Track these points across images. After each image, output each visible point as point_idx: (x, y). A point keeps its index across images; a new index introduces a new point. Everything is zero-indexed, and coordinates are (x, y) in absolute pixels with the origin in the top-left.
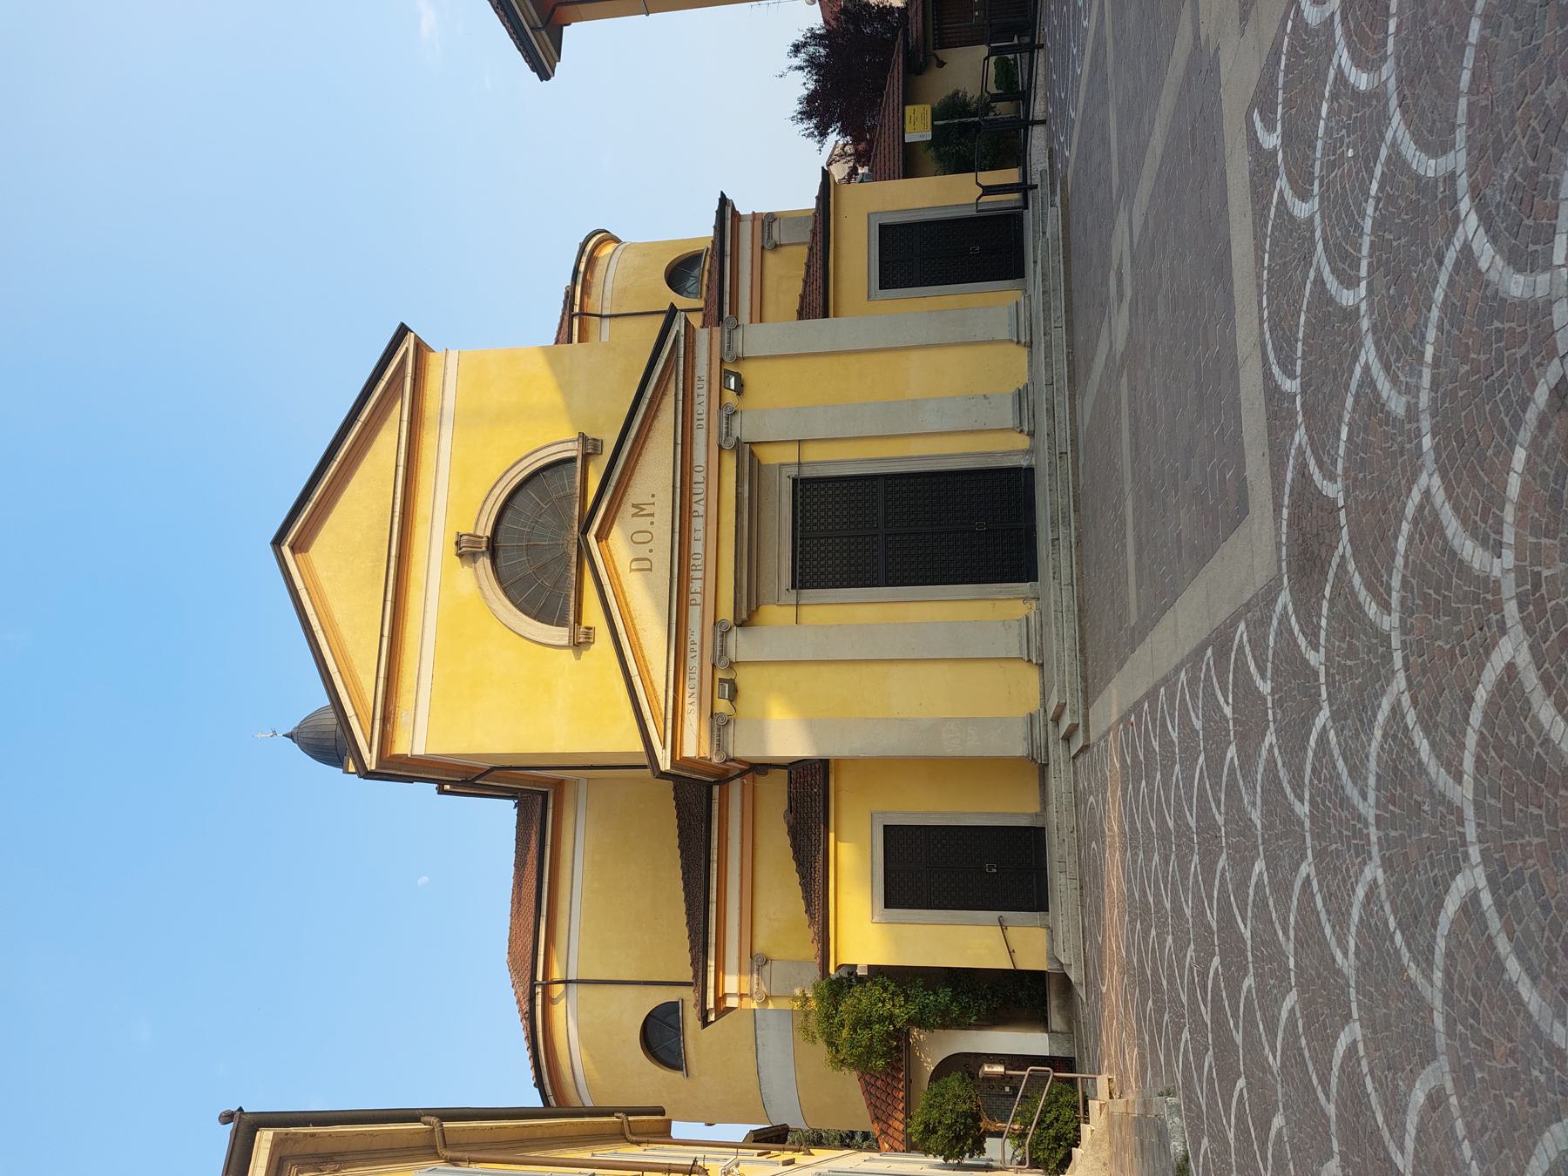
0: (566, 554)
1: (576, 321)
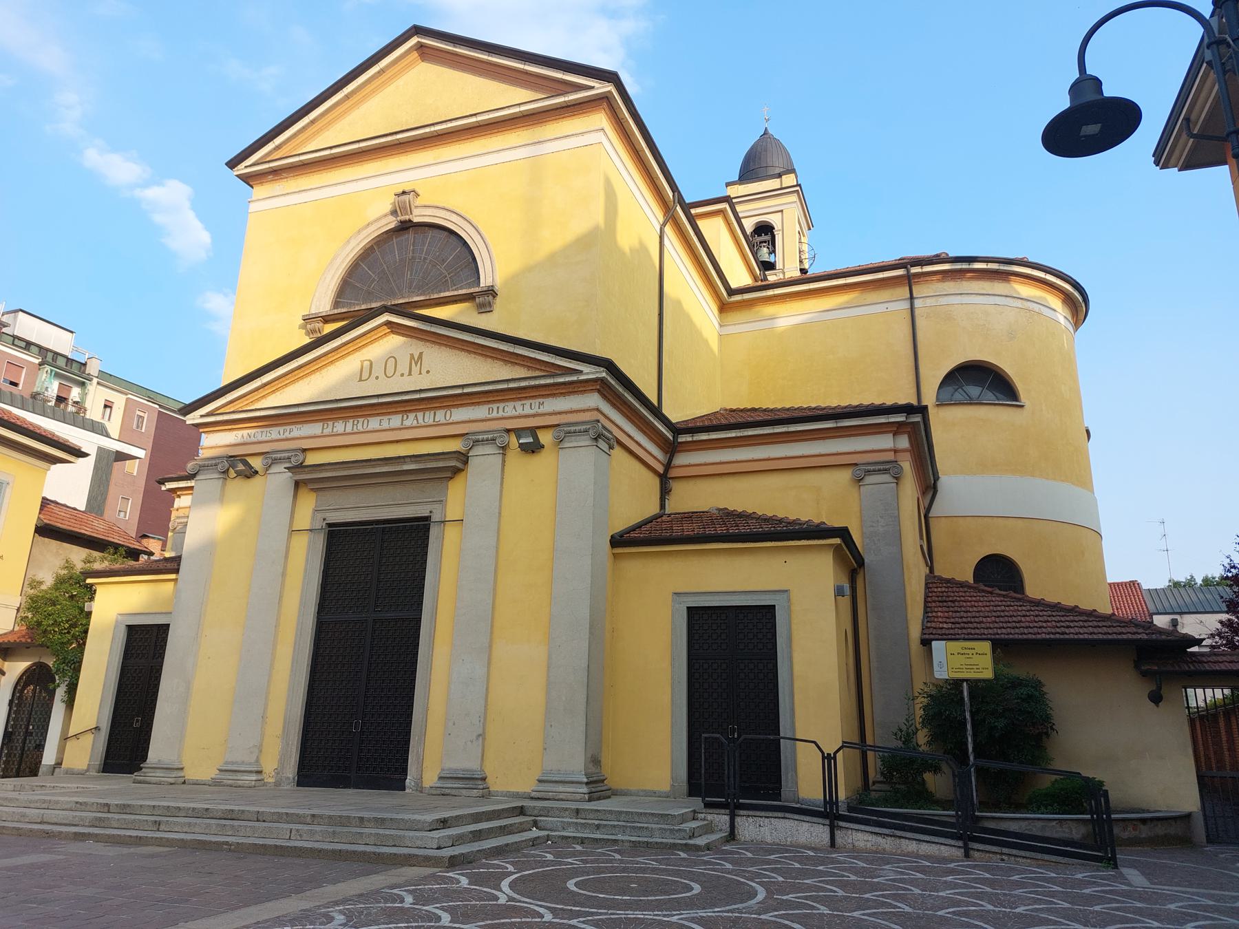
0: (392, 294)
1: (900, 272)
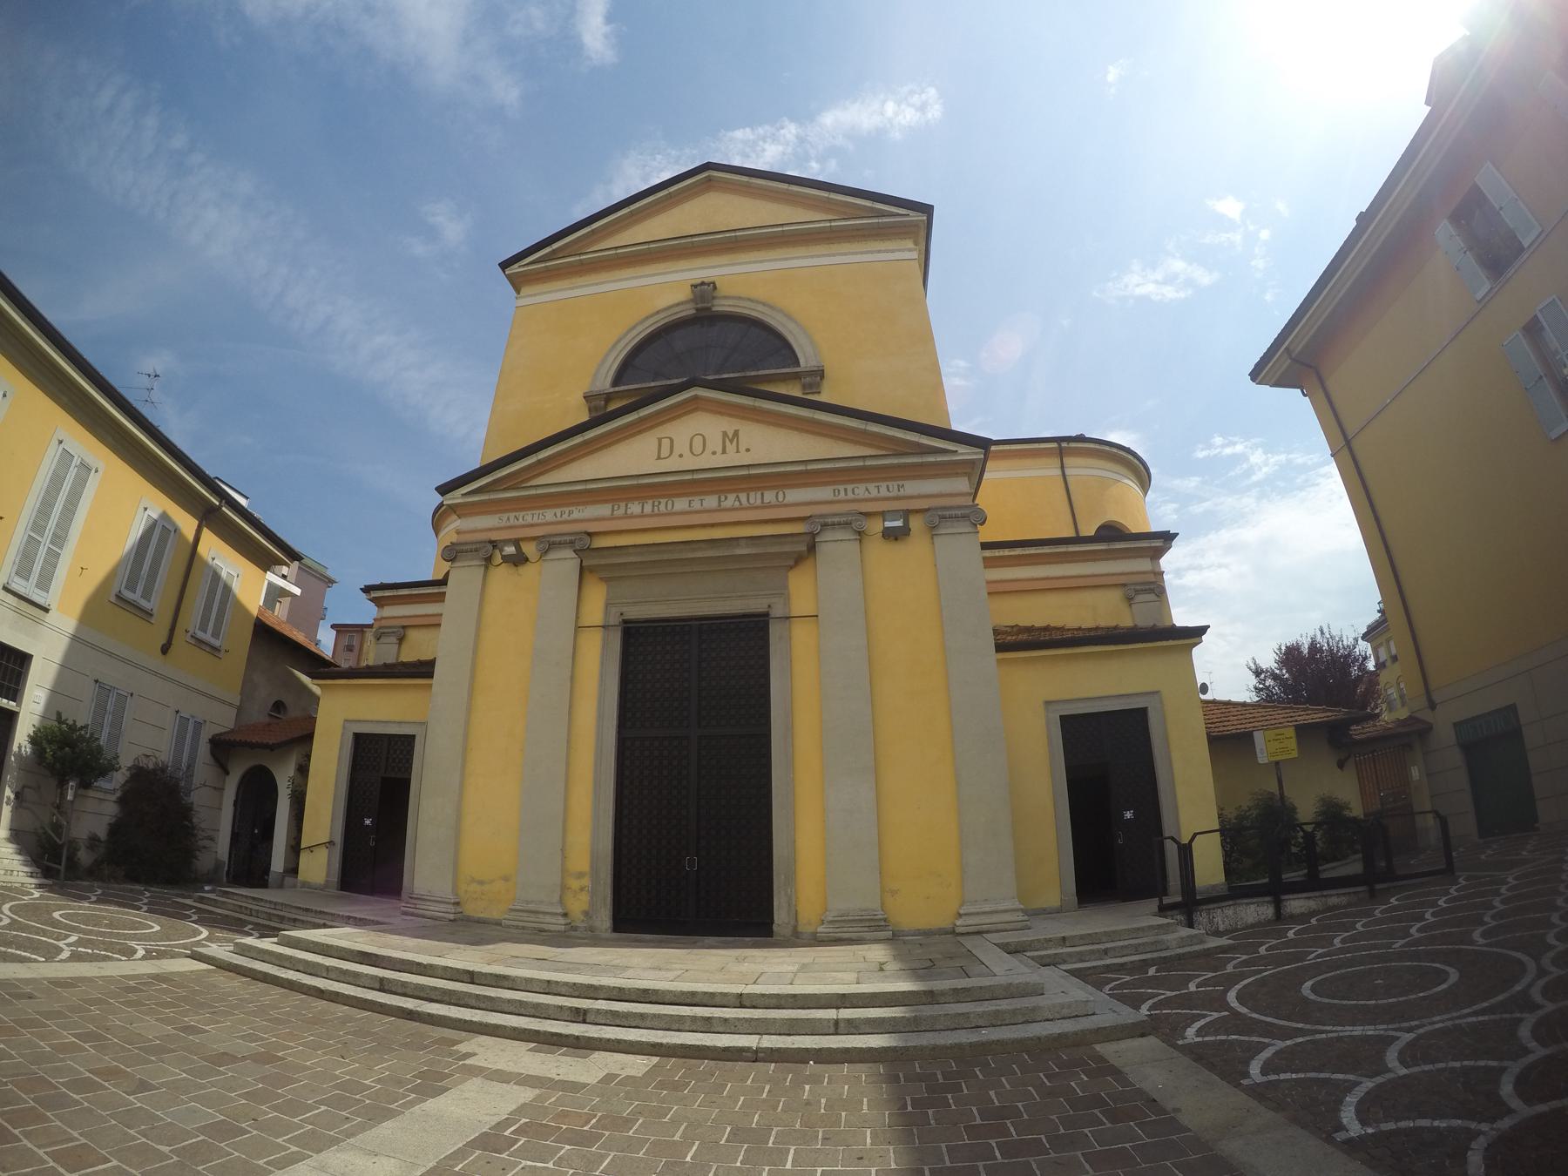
1: (1054, 445)
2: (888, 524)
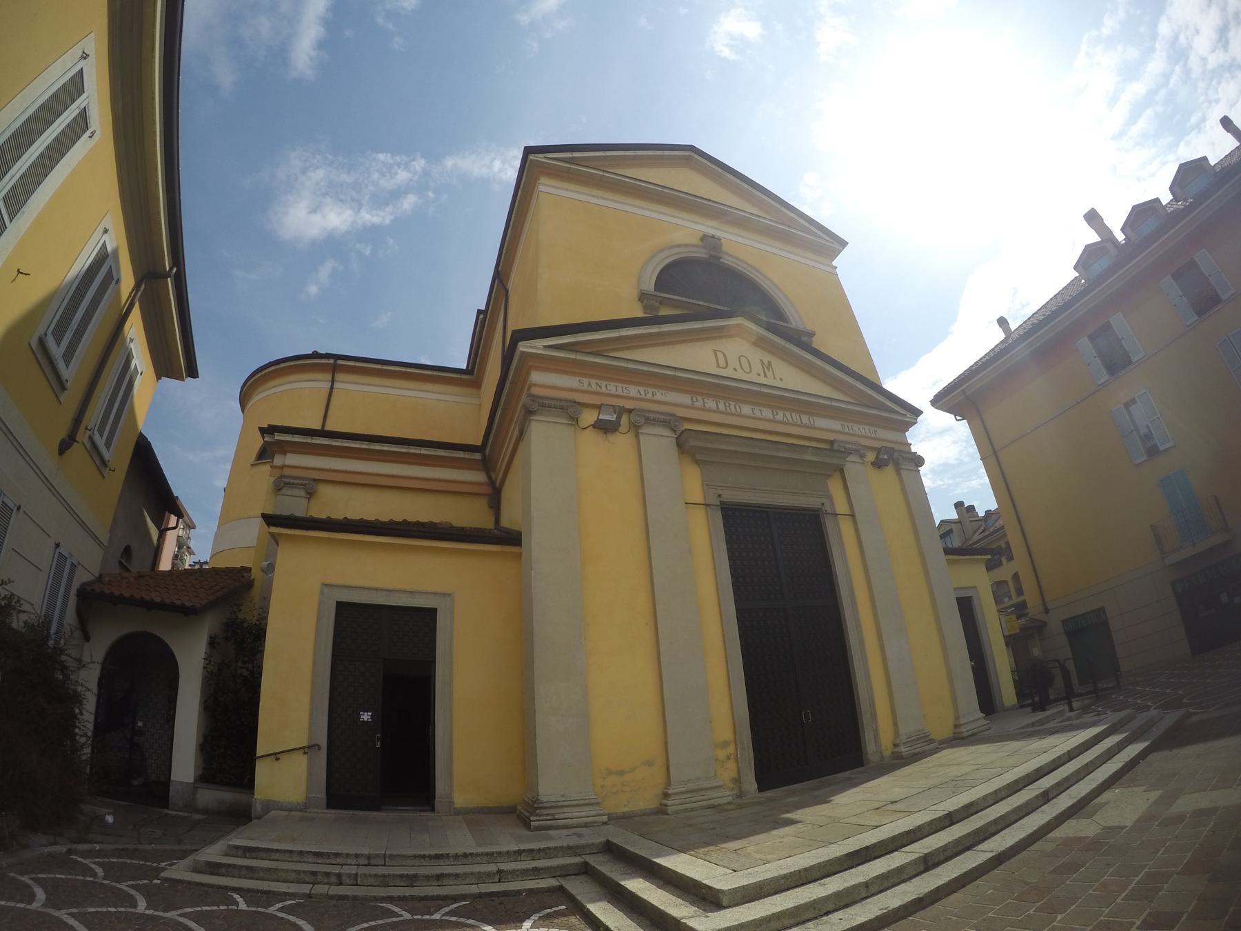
2: (601, 417)
